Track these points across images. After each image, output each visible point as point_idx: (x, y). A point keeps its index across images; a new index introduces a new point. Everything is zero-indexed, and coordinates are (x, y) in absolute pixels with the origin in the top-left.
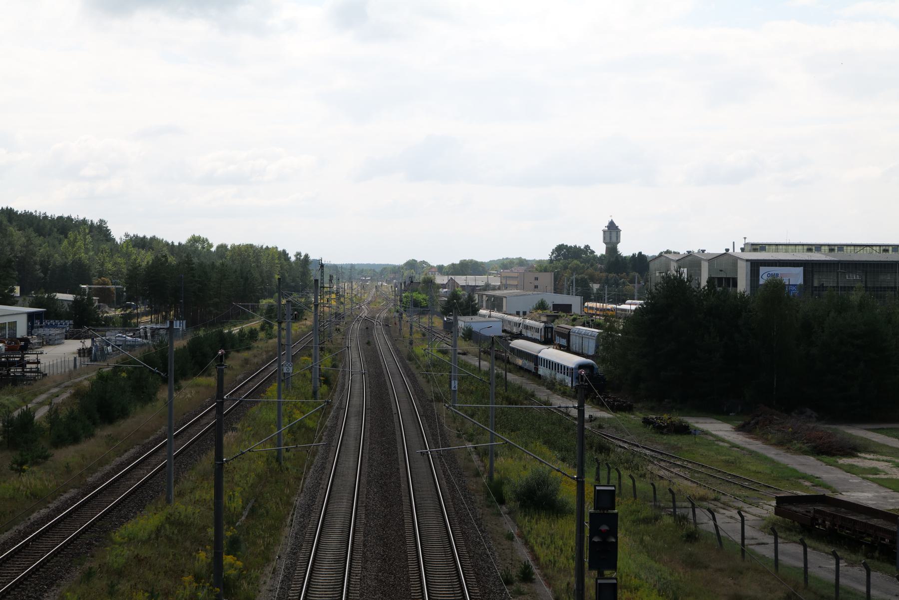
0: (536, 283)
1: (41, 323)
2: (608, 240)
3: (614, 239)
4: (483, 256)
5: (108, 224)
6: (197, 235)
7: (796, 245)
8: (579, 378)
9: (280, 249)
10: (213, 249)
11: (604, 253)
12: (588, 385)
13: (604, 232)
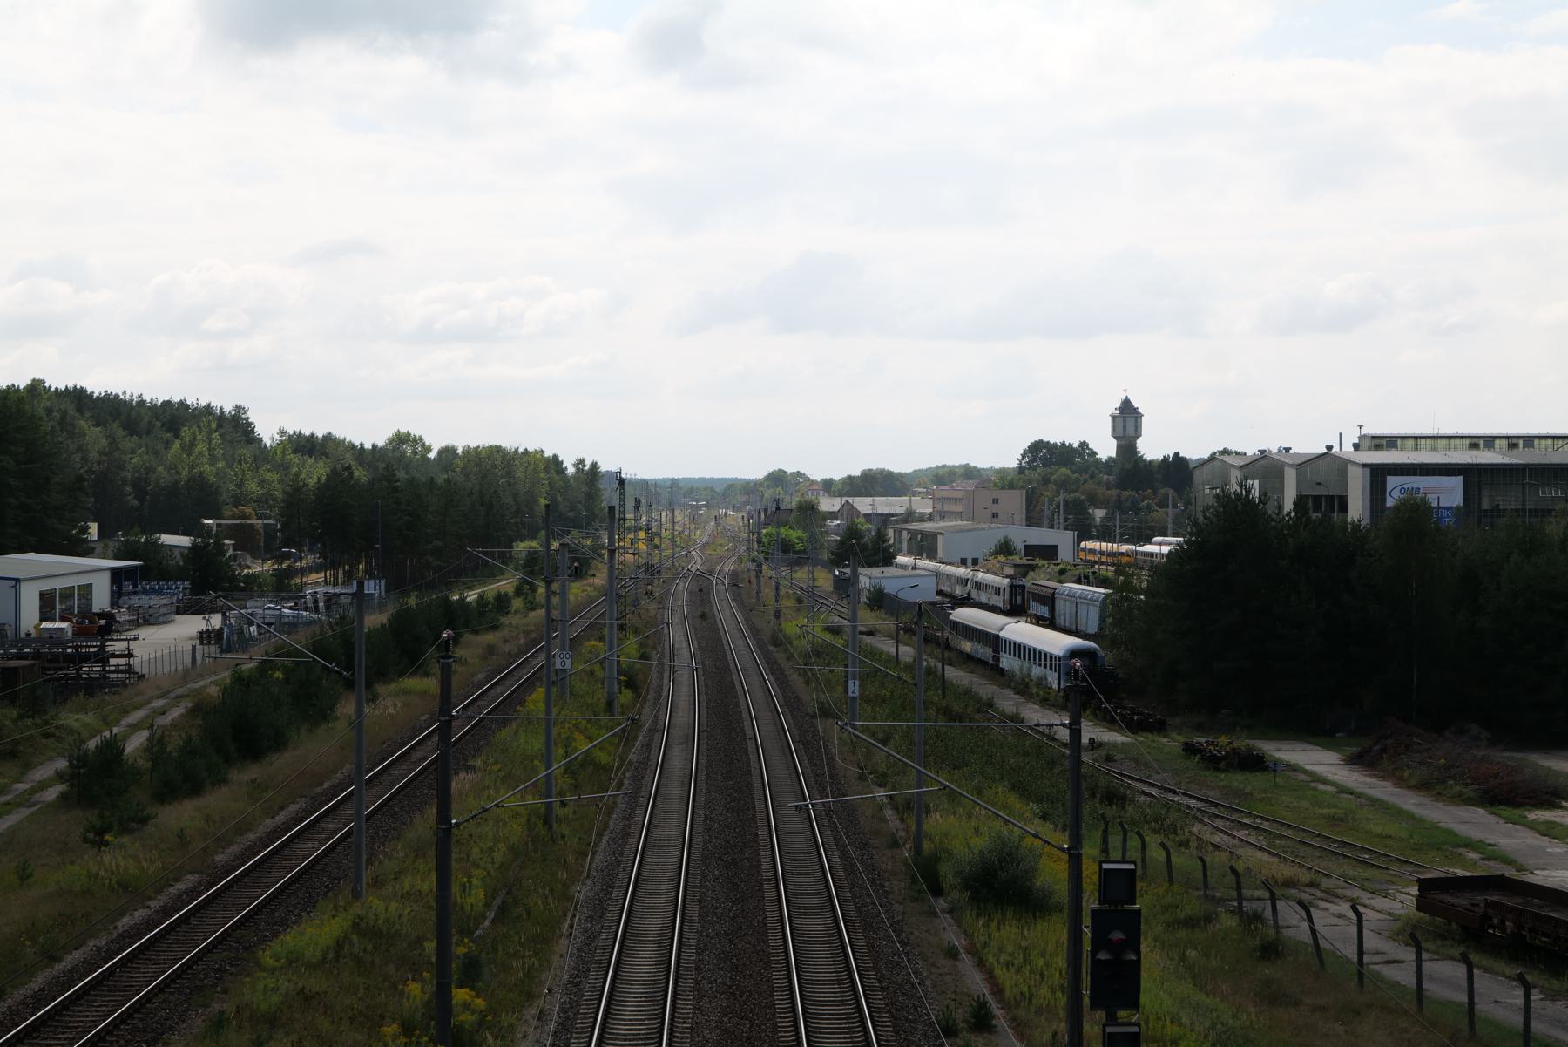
0: (996, 508)
1: (135, 586)
2: (1120, 432)
3: (1130, 431)
5: (249, 414)
6: (403, 431)
7: (1450, 437)
10: (432, 455)
11: (1114, 455)
12: (1088, 685)
13: (1114, 417)
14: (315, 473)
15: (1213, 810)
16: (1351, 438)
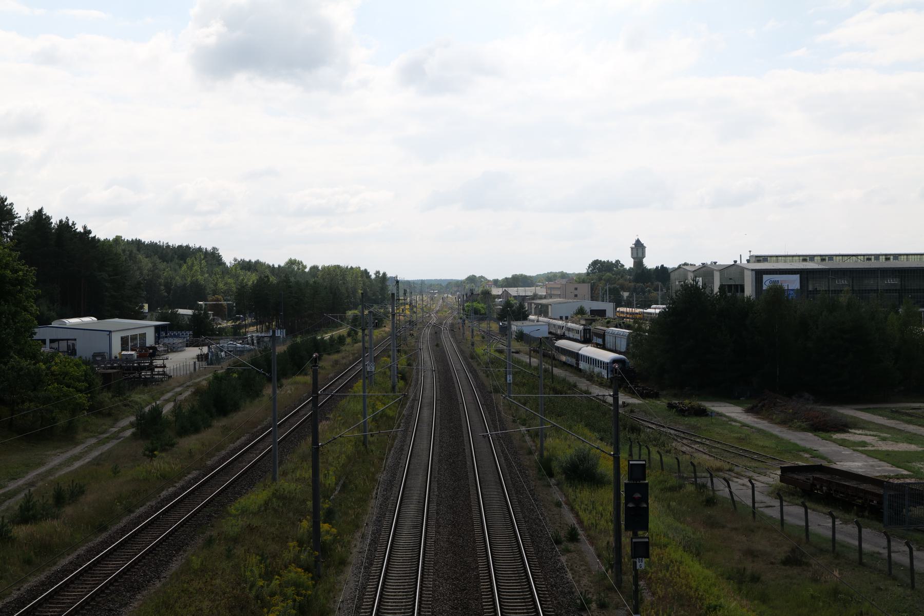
2: (635, 256)
3: (640, 255)
4: (531, 271)
7: (793, 256)
8: (614, 371)
9: (362, 269)
10: (307, 270)
12: (622, 376)
14: (251, 279)
15: (682, 435)
16: (746, 257)
